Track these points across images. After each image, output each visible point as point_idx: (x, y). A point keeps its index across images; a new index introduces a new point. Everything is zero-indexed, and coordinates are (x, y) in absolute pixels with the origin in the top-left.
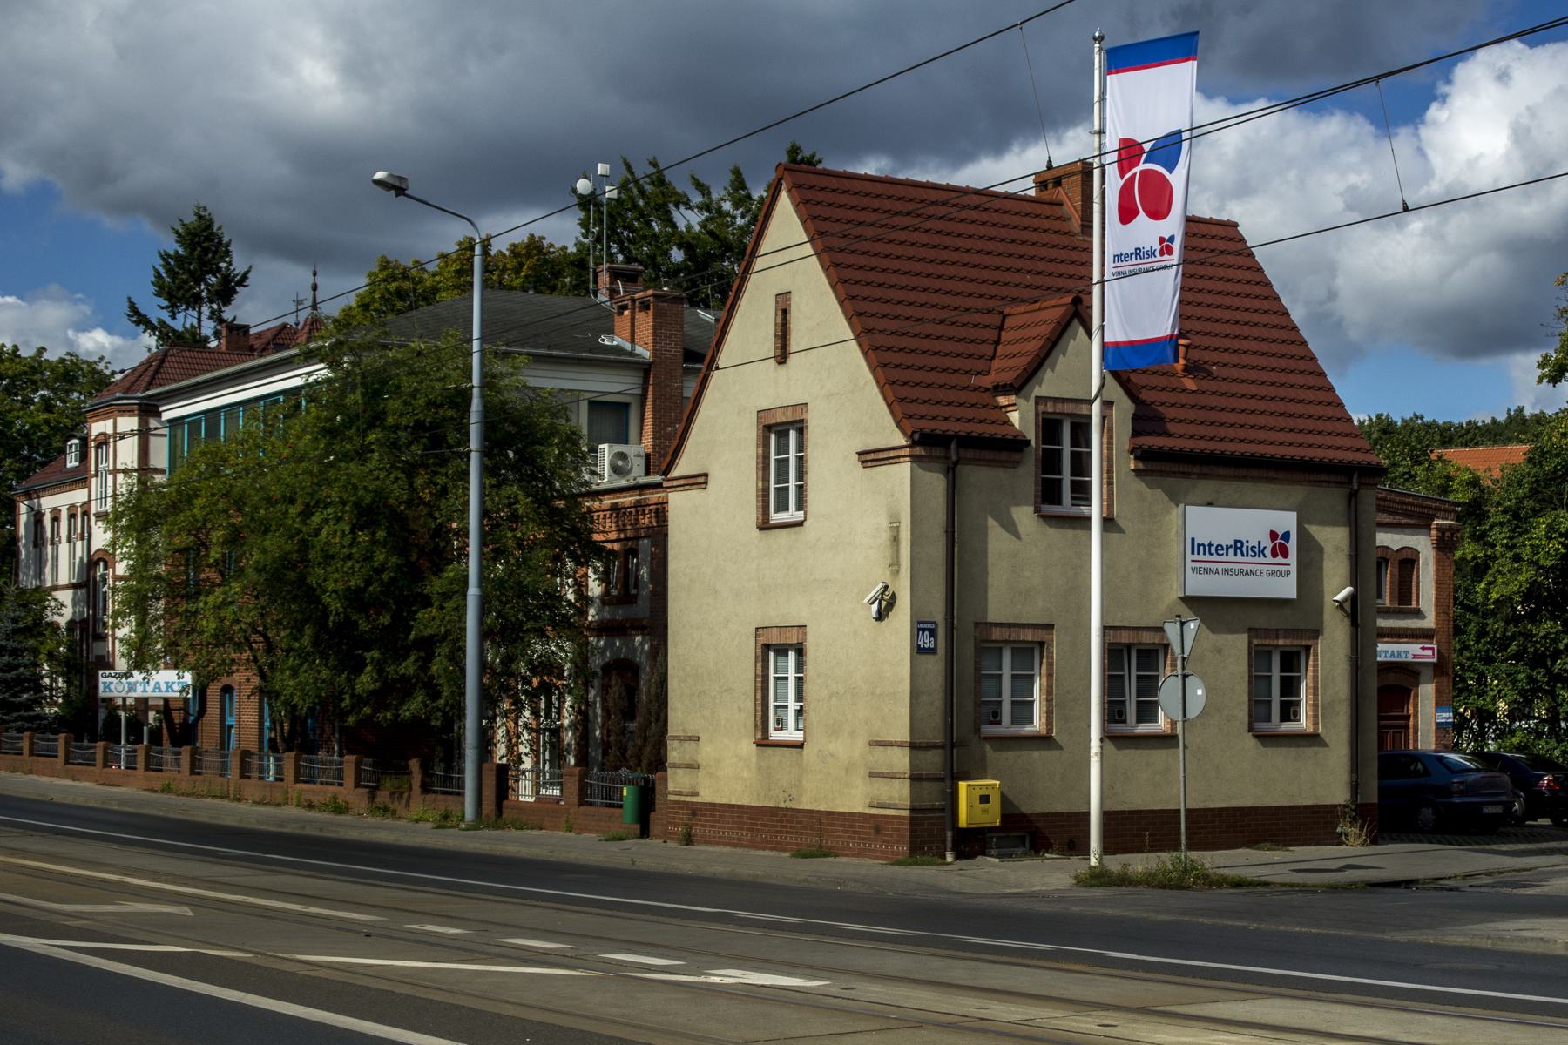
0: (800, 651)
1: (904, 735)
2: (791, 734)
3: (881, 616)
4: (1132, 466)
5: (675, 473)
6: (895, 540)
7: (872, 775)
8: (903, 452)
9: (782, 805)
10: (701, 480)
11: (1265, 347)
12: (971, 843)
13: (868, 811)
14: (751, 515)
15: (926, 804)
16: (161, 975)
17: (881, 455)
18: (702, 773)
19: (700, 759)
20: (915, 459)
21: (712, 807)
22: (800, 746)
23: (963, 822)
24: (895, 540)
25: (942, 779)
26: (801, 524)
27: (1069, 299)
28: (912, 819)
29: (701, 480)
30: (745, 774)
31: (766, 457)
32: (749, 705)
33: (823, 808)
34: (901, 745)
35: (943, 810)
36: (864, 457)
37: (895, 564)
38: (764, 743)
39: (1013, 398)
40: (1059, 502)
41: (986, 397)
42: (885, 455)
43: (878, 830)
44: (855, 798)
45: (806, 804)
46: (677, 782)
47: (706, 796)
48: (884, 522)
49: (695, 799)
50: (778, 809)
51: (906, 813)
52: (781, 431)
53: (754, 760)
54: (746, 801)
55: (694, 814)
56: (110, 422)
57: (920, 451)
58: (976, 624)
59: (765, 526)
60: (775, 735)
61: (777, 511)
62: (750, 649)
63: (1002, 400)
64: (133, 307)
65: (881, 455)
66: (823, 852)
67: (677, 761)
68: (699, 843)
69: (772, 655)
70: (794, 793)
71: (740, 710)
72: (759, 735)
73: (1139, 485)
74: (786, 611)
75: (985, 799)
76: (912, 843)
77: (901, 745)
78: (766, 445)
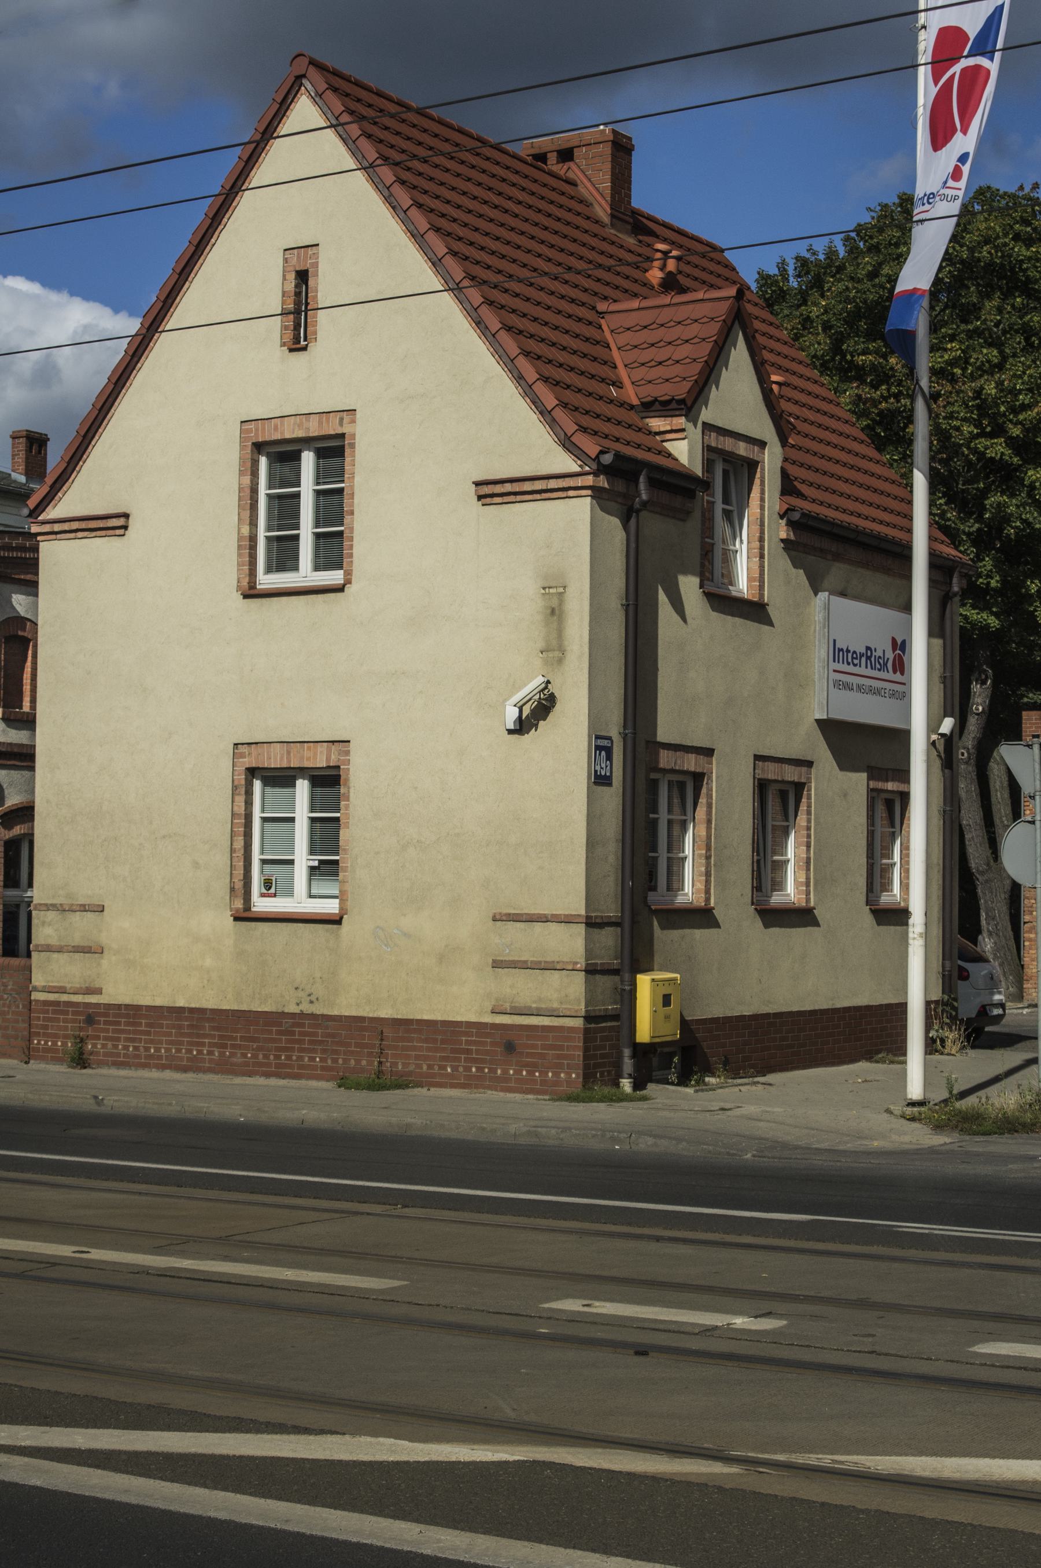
0: (328, 782)
1: (578, 907)
2: (300, 898)
3: (522, 727)
4: (783, 535)
5: (53, 512)
6: (555, 613)
8: (579, 482)
9: (292, 1008)
10: (121, 522)
12: (655, 1064)
13: (489, 1019)
14: (228, 572)
15: (600, 1008)
16: (540, 1457)
17: (527, 486)
18: (106, 962)
19: (104, 939)
20: (597, 493)
21: (132, 1013)
22: (336, 921)
23: (644, 1033)
24: (555, 613)
25: (616, 972)
26: (340, 589)
27: (732, 291)
28: (586, 1031)
29: (121, 522)
30: (208, 962)
31: (254, 490)
32: (220, 860)
33: (385, 1012)
34: (567, 920)
35: (615, 1017)
36: (486, 490)
37: (554, 651)
38: (245, 916)
39: (681, 421)
41: (633, 417)
42: (539, 485)
43: (510, 1048)
44: (464, 999)
45: (346, 1006)
47: (119, 989)
48: (529, 589)
50: (283, 1014)
51: (579, 1023)
52: (284, 455)
54: (209, 1001)
55: (90, 1020)
57: (603, 482)
58: (648, 742)
59: (251, 593)
60: (261, 904)
61: (269, 570)
62: (222, 773)
63: (657, 424)
65: (527, 486)
66: (378, 1083)
67: (54, 941)
68: (101, 1064)
69: (257, 784)
70: (319, 990)
71: (196, 865)
72: (239, 904)
73: (784, 562)
74: (296, 720)
75: (282, 996)
76: (586, 1067)
77: (567, 920)
78: (255, 474)
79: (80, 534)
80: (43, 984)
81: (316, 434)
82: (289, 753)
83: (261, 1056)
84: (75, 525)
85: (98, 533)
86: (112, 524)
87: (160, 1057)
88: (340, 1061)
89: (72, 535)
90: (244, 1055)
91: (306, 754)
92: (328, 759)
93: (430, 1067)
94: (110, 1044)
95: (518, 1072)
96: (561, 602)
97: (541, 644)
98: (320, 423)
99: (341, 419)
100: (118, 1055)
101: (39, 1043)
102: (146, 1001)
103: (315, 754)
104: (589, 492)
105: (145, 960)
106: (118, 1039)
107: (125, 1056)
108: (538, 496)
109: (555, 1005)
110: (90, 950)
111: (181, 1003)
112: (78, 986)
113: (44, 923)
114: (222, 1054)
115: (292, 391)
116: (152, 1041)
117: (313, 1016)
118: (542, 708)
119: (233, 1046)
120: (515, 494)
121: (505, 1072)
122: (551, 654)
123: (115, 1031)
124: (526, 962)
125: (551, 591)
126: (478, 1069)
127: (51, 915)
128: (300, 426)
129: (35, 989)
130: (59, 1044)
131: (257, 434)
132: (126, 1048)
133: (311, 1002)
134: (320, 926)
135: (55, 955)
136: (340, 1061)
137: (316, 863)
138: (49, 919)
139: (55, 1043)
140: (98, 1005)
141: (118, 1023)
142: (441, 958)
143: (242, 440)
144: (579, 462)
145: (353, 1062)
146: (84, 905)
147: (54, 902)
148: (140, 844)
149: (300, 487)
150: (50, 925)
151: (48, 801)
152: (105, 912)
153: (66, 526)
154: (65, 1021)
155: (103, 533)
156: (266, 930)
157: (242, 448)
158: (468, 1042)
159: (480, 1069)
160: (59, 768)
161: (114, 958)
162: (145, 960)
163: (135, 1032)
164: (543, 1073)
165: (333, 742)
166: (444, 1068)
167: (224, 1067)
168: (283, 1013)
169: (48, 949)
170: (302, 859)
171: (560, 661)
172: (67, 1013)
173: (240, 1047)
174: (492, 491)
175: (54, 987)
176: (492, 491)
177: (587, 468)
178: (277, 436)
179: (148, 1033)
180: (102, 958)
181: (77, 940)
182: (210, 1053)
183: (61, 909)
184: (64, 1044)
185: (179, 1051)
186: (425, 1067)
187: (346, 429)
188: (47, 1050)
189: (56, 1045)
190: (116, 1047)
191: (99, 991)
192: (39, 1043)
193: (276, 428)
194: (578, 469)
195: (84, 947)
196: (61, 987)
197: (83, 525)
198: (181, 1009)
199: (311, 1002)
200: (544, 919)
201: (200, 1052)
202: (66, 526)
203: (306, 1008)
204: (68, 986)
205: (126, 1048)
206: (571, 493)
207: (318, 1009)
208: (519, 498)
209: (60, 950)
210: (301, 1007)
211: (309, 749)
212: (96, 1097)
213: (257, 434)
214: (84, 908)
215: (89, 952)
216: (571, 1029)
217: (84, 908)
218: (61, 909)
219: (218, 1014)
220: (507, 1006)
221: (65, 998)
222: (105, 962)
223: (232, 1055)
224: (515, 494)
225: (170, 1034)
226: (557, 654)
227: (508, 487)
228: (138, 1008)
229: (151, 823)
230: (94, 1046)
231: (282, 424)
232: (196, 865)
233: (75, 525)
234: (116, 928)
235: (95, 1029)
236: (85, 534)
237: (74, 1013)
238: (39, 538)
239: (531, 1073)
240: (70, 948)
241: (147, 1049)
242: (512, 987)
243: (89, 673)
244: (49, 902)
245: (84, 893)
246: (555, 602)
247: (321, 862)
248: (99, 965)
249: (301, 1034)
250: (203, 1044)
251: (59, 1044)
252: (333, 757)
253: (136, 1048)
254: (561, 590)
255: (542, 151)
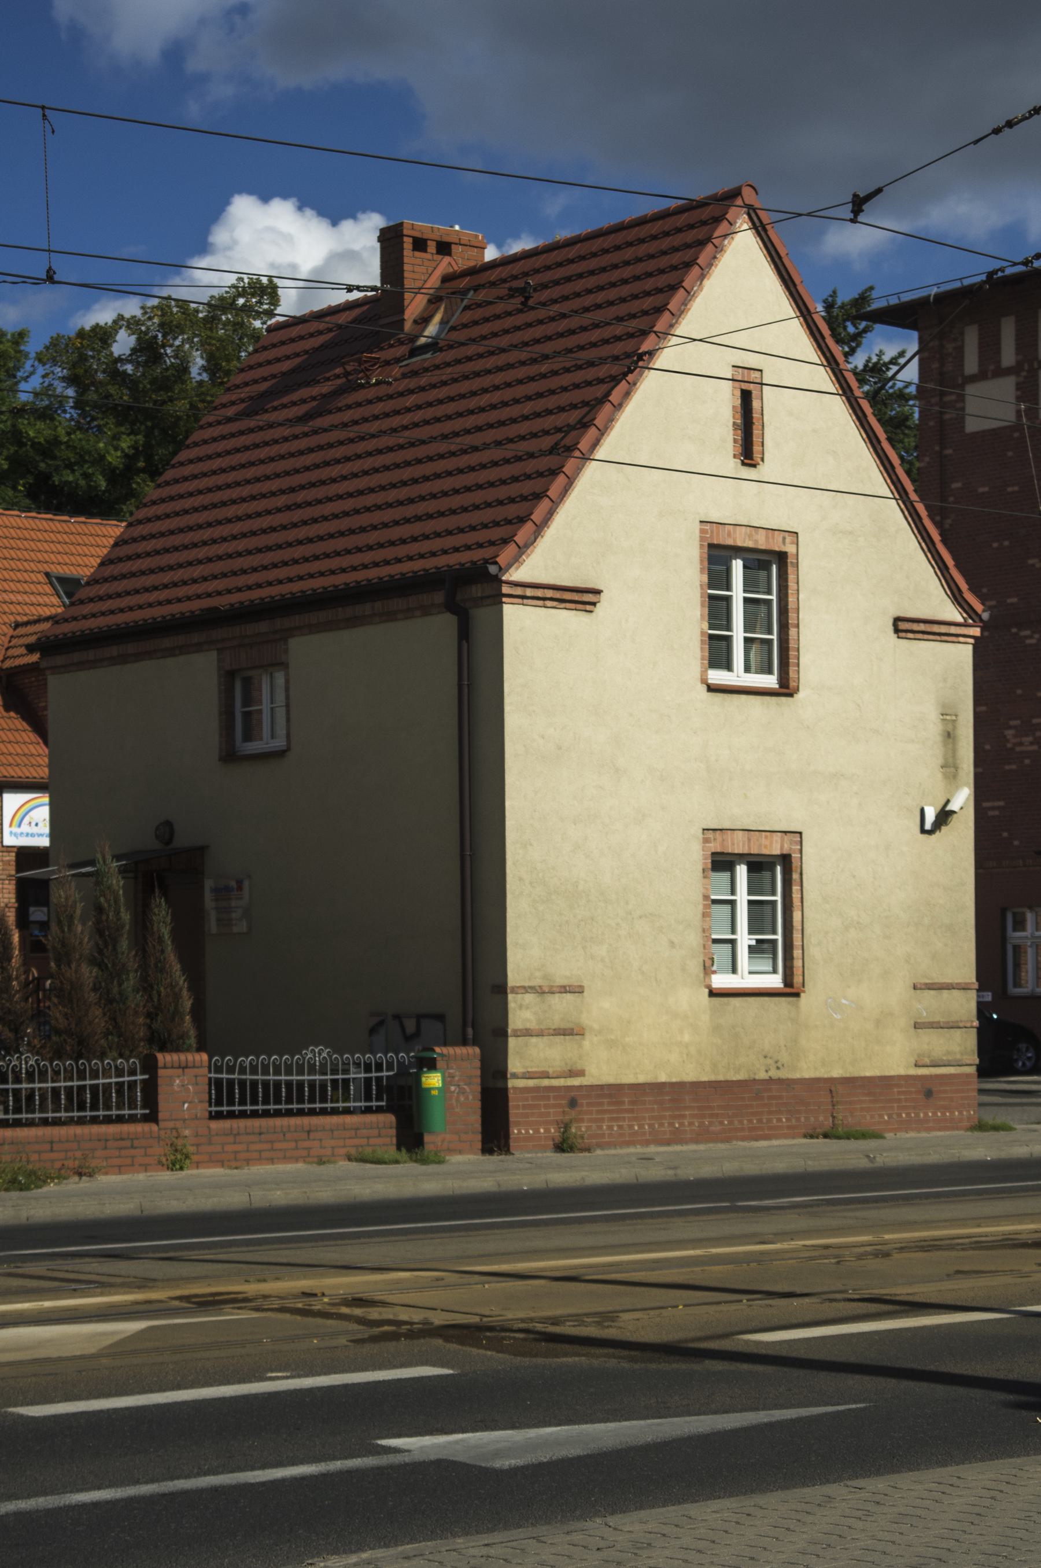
7: (917, 1026)
9: (762, 1075)
10: (903, 626)
11: (493, 416)
17: (936, 628)
19: (586, 1020)
21: (613, 1093)
24: (949, 736)
30: (687, 1037)
33: (836, 1073)
40: (728, 667)
43: (929, 1094)
44: (894, 1056)
45: (807, 1070)
46: (527, 1059)
47: (602, 1068)
48: (932, 715)
49: (576, 1082)
50: (754, 1081)
53: (705, 1018)
54: (690, 1073)
55: (573, 1103)
56: (405, 239)
62: (695, 856)
64: (757, 193)
65: (936, 628)
67: (533, 1025)
70: (784, 1057)
71: (672, 944)
74: (762, 809)
79: (549, 603)
80: (524, 1070)
81: (763, 547)
82: (749, 840)
83: (736, 1122)
84: (549, 593)
85: (568, 605)
86: (581, 598)
87: (644, 1133)
88: (803, 1119)
89: (540, 603)
90: (722, 1123)
91: (764, 841)
92: (782, 847)
93: (872, 1117)
94: (594, 1125)
95: (935, 1114)
96: (955, 728)
97: (940, 761)
98: (767, 537)
99: (784, 538)
100: (603, 1135)
101: (520, 1132)
102: (629, 1079)
103: (771, 843)
104: (972, 641)
105: (627, 1039)
106: (602, 1120)
107: (610, 1135)
108: (938, 638)
109: (958, 1057)
110: (571, 1032)
111: (663, 1078)
112: (559, 1069)
113: (521, 1007)
114: (701, 1124)
115: (751, 506)
116: (636, 1119)
117: (780, 1081)
118: (944, 816)
119: (712, 1116)
120: (923, 632)
121: (926, 1114)
122: (948, 770)
123: (598, 1112)
124: (939, 1022)
125: (948, 718)
126: (907, 1114)
127: (529, 998)
128: (750, 536)
129: (515, 1076)
130: (542, 1131)
131: (712, 536)
132: (610, 1128)
133: (778, 1068)
134: (783, 999)
135: (534, 1040)
136: (803, 1119)
137: (753, 943)
138: (527, 1001)
139: (537, 1131)
140: (580, 1087)
141: (601, 1104)
142: (878, 1023)
143: (702, 539)
144: (965, 615)
145: (812, 1119)
146: (564, 987)
147: (531, 984)
148: (618, 924)
149: (750, 594)
150: (527, 1008)
151: (521, 879)
152: (585, 993)
153: (539, 593)
154: (546, 1106)
155: (573, 606)
156: (738, 1005)
157: (701, 546)
158: (899, 1093)
159: (908, 1114)
160: (531, 845)
161: (595, 1039)
162: (627, 1039)
163: (618, 1111)
164: (952, 1113)
165: (785, 832)
166: (881, 1116)
167: (702, 1136)
168: (755, 1080)
169: (528, 1033)
170: (745, 939)
171: (955, 776)
172: (548, 1098)
173: (717, 1115)
174: (903, 627)
175: (536, 1072)
176: (903, 627)
177: (970, 621)
178: (729, 542)
179: (632, 1111)
180: (583, 1039)
181: (556, 1021)
182: (691, 1124)
183: (539, 991)
184: (547, 1131)
185: (661, 1125)
186: (868, 1117)
187: (790, 549)
188: (530, 1138)
189: (539, 1132)
190: (600, 1128)
191: (581, 1073)
192: (520, 1132)
193: (729, 535)
194: (960, 619)
195: (565, 1030)
196: (543, 1072)
197: (558, 595)
198: (663, 1085)
199: (778, 1068)
200: (949, 987)
201: (681, 1124)
202: (539, 593)
203: (774, 1074)
204: (551, 1070)
205: (610, 1128)
206: (961, 639)
207: (783, 1074)
208: (926, 637)
209: (540, 1034)
210: (770, 1073)
211: (766, 837)
212: (868, 1157)
213: (712, 536)
214: (565, 990)
215: (571, 1034)
216: (968, 1075)
217: (565, 990)
218: (539, 991)
219: (696, 1086)
220: (927, 1061)
221: (546, 1082)
222: (586, 1043)
223: (711, 1124)
224: (923, 632)
225: (653, 1110)
226: (952, 770)
227: (922, 627)
228: (681, 1085)
229: (627, 903)
230: (579, 1128)
231: (735, 532)
232: (672, 944)
233: (549, 593)
234: (598, 1009)
235: (585, 1109)
236: (555, 604)
237: (555, 1098)
238: (504, 599)
239: (943, 1114)
240: (551, 1031)
241: (631, 1127)
242: (928, 1044)
243: (560, 748)
244: (526, 984)
245: (563, 972)
246: (950, 728)
247: (758, 941)
248: (580, 1046)
249: (770, 1098)
250: (683, 1116)
251: (542, 1131)
252: (786, 846)
253: (620, 1127)
254: (954, 718)
255: (425, 237)
